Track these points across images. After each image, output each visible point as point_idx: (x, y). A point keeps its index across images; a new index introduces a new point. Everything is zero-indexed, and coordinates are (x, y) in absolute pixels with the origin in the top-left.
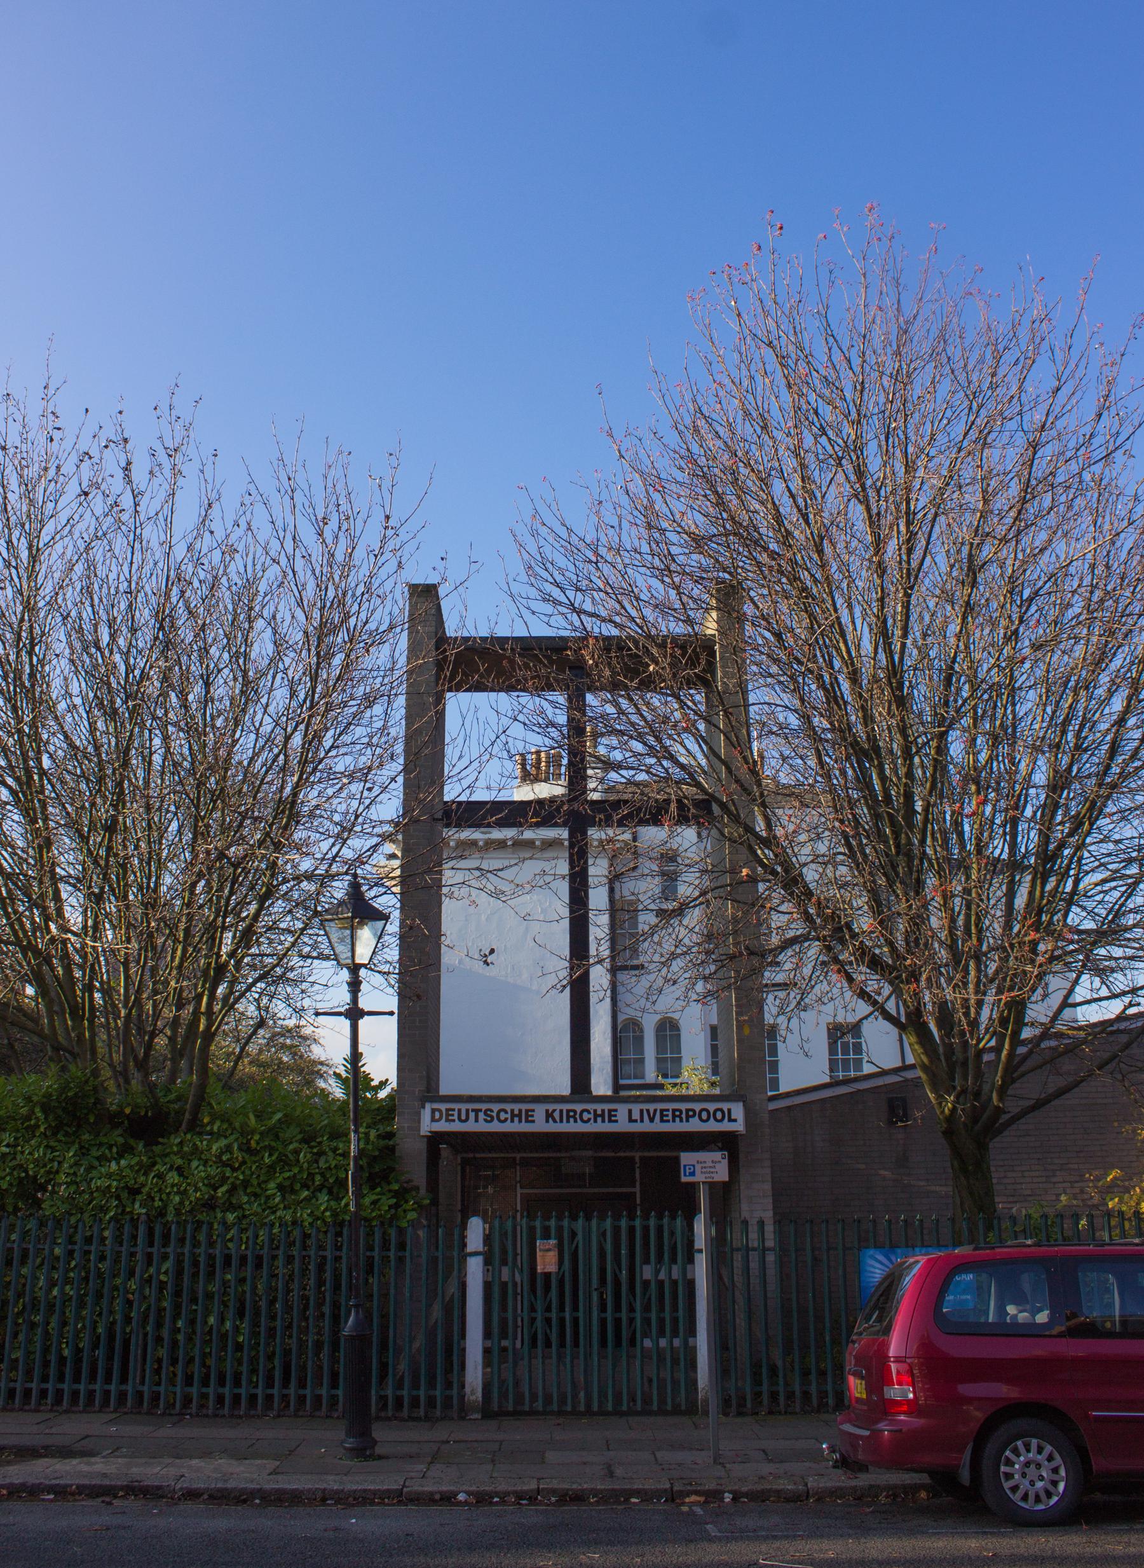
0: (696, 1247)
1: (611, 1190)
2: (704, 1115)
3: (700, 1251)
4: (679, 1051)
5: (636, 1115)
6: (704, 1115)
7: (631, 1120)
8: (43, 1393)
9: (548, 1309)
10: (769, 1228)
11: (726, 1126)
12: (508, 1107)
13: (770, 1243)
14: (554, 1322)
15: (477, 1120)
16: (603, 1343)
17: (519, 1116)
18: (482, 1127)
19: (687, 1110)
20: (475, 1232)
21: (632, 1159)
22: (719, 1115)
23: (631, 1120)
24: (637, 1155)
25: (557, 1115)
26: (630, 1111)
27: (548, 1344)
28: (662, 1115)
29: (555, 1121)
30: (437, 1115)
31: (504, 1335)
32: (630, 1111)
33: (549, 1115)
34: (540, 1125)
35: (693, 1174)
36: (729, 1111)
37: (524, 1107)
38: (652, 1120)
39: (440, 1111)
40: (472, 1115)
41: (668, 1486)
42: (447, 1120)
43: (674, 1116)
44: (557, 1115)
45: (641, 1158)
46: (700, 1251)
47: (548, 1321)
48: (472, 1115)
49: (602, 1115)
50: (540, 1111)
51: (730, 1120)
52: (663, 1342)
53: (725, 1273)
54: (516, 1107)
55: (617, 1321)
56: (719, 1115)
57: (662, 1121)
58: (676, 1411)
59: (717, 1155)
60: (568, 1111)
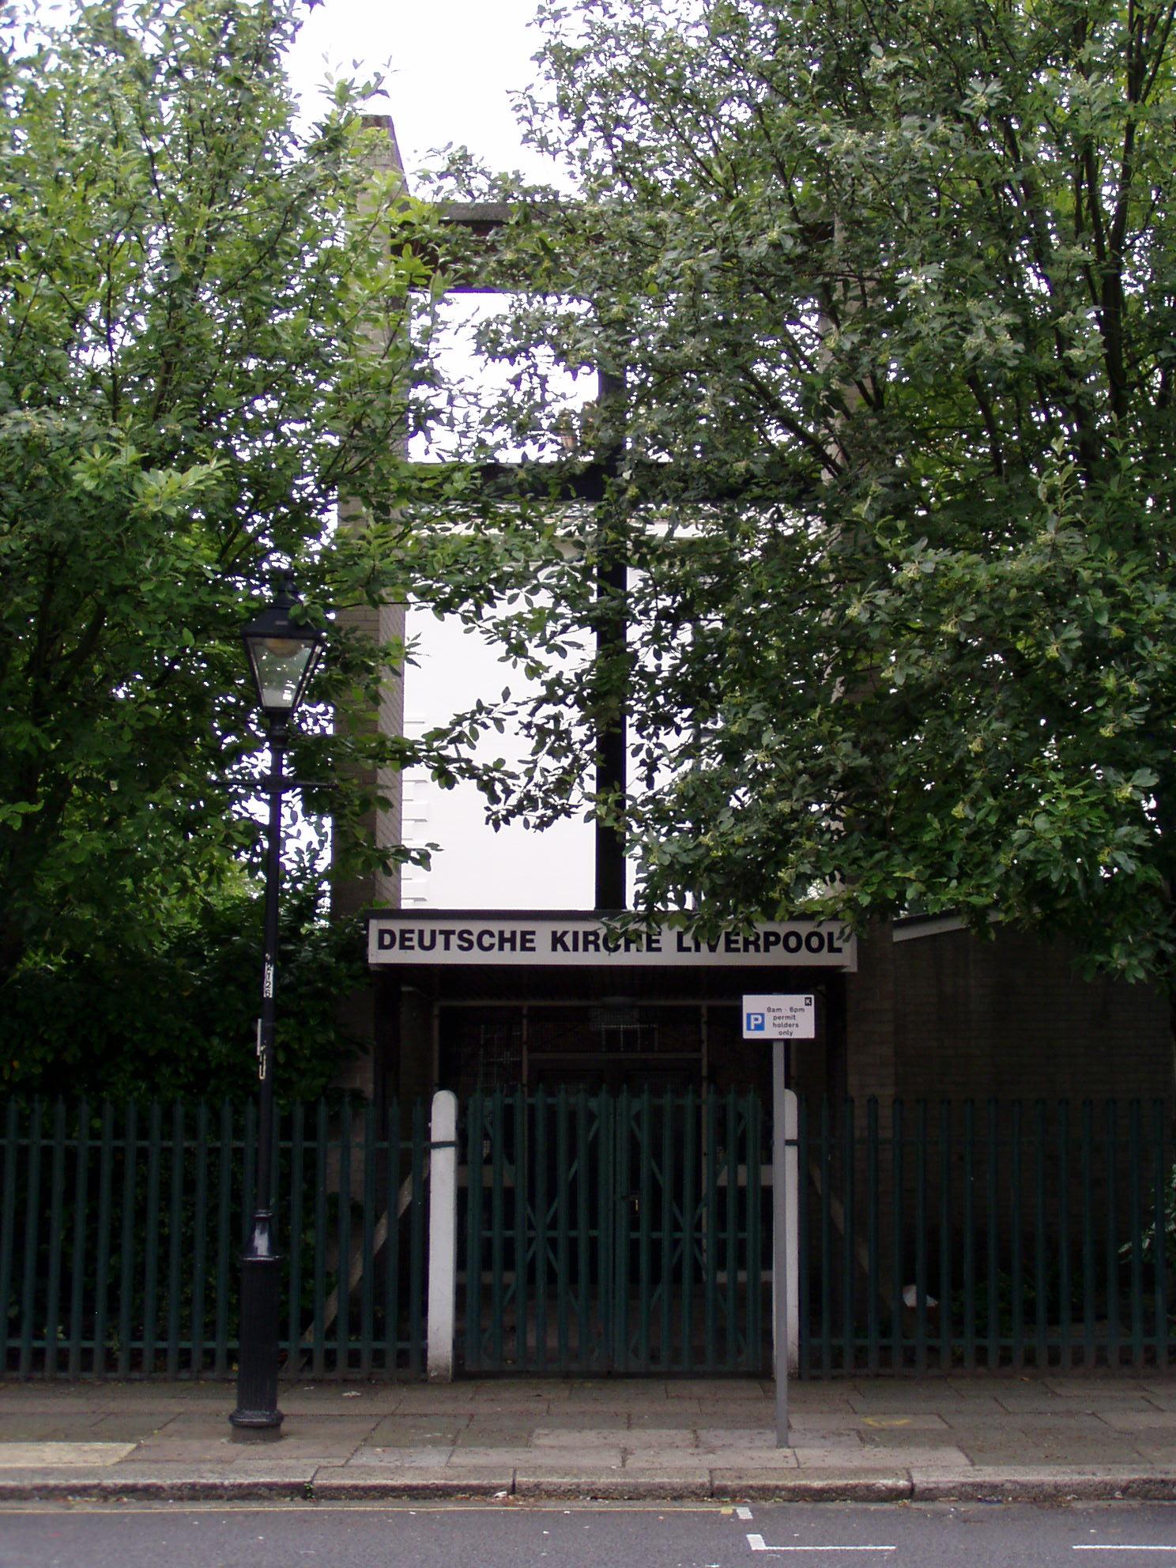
0: (436, 1137)
1: (436, 1055)
3: (789, 1143)
7: (681, 948)
10: (886, 1113)
11: (825, 959)
12: (495, 927)
13: (887, 1134)
15: (447, 947)
16: (634, 1275)
17: (512, 940)
20: (444, 1113)
21: (697, 1008)
23: (681, 948)
24: (704, 1004)
29: (566, 948)
30: (387, 939)
31: (487, 1263)
33: (557, 940)
34: (543, 955)
35: (760, 1027)
37: (520, 927)
39: (391, 933)
40: (440, 939)
41: (706, 1480)
42: (403, 947)
45: (710, 1008)
46: (789, 1143)
48: (440, 939)
50: (543, 933)
51: (832, 949)
52: (742, 1276)
54: (508, 927)
55: (656, 1245)
57: (728, 949)
58: (750, 1376)
59: (798, 1000)
60: (586, 934)
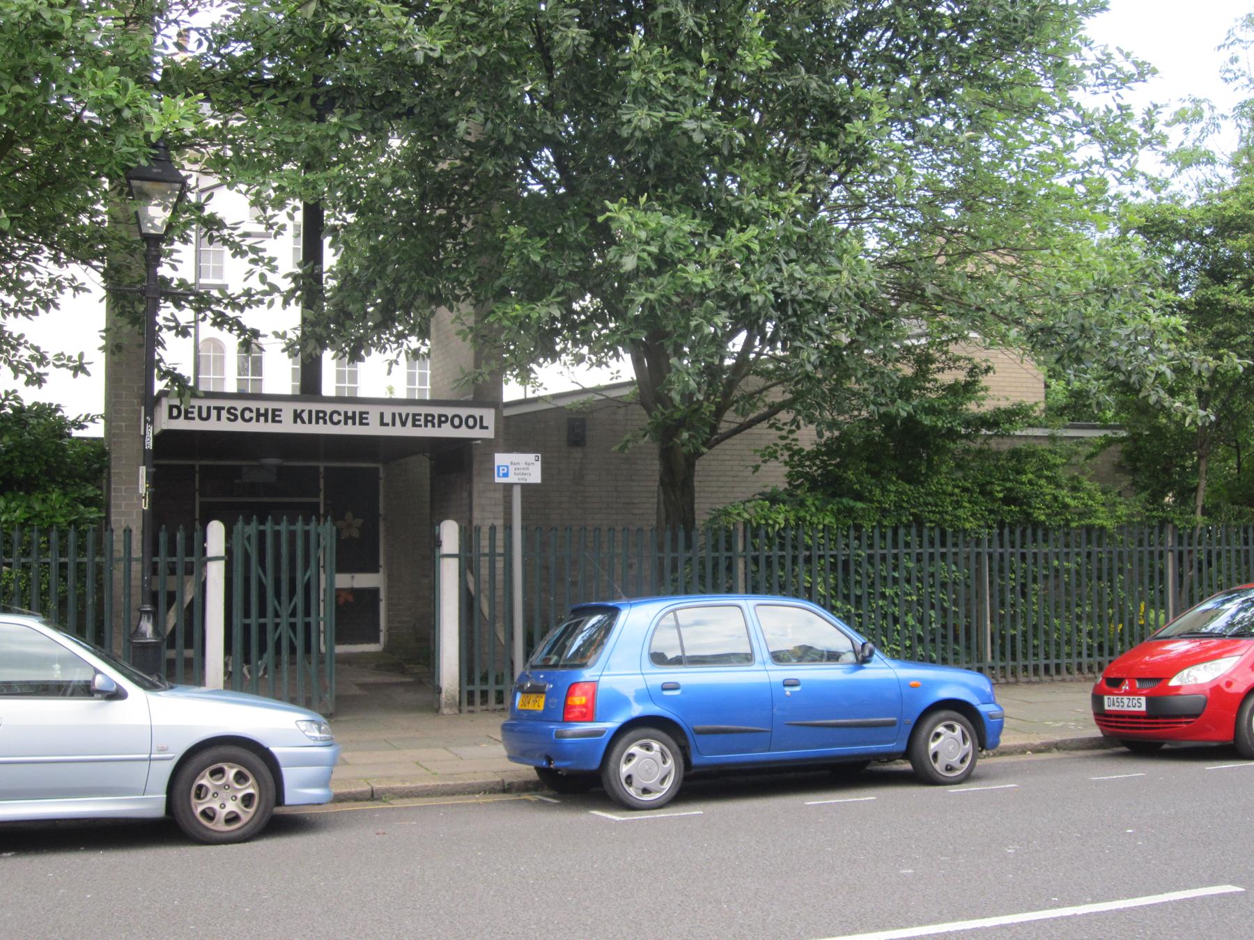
2: (457, 421)
4: (222, 373)
5: (388, 419)
6: (457, 421)
7: (382, 424)
8: (484, 694)
9: (293, 614)
14: (300, 628)
15: (219, 418)
17: (266, 415)
18: (225, 426)
19: (440, 416)
22: (471, 422)
23: (382, 424)
24: (322, 465)
25: (305, 416)
26: (382, 415)
27: (293, 650)
28: (414, 420)
29: (303, 422)
30: (175, 412)
32: (382, 415)
33: (297, 416)
35: (506, 475)
36: (481, 418)
38: (404, 424)
40: (214, 413)
42: (186, 418)
43: (426, 421)
44: (305, 416)
45: (326, 468)
47: (293, 626)
48: (214, 413)
49: (353, 418)
51: (482, 427)
53: (470, 579)
56: (471, 422)
57: (414, 425)
59: (531, 457)
60: (318, 412)
